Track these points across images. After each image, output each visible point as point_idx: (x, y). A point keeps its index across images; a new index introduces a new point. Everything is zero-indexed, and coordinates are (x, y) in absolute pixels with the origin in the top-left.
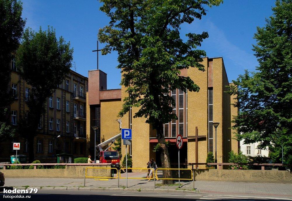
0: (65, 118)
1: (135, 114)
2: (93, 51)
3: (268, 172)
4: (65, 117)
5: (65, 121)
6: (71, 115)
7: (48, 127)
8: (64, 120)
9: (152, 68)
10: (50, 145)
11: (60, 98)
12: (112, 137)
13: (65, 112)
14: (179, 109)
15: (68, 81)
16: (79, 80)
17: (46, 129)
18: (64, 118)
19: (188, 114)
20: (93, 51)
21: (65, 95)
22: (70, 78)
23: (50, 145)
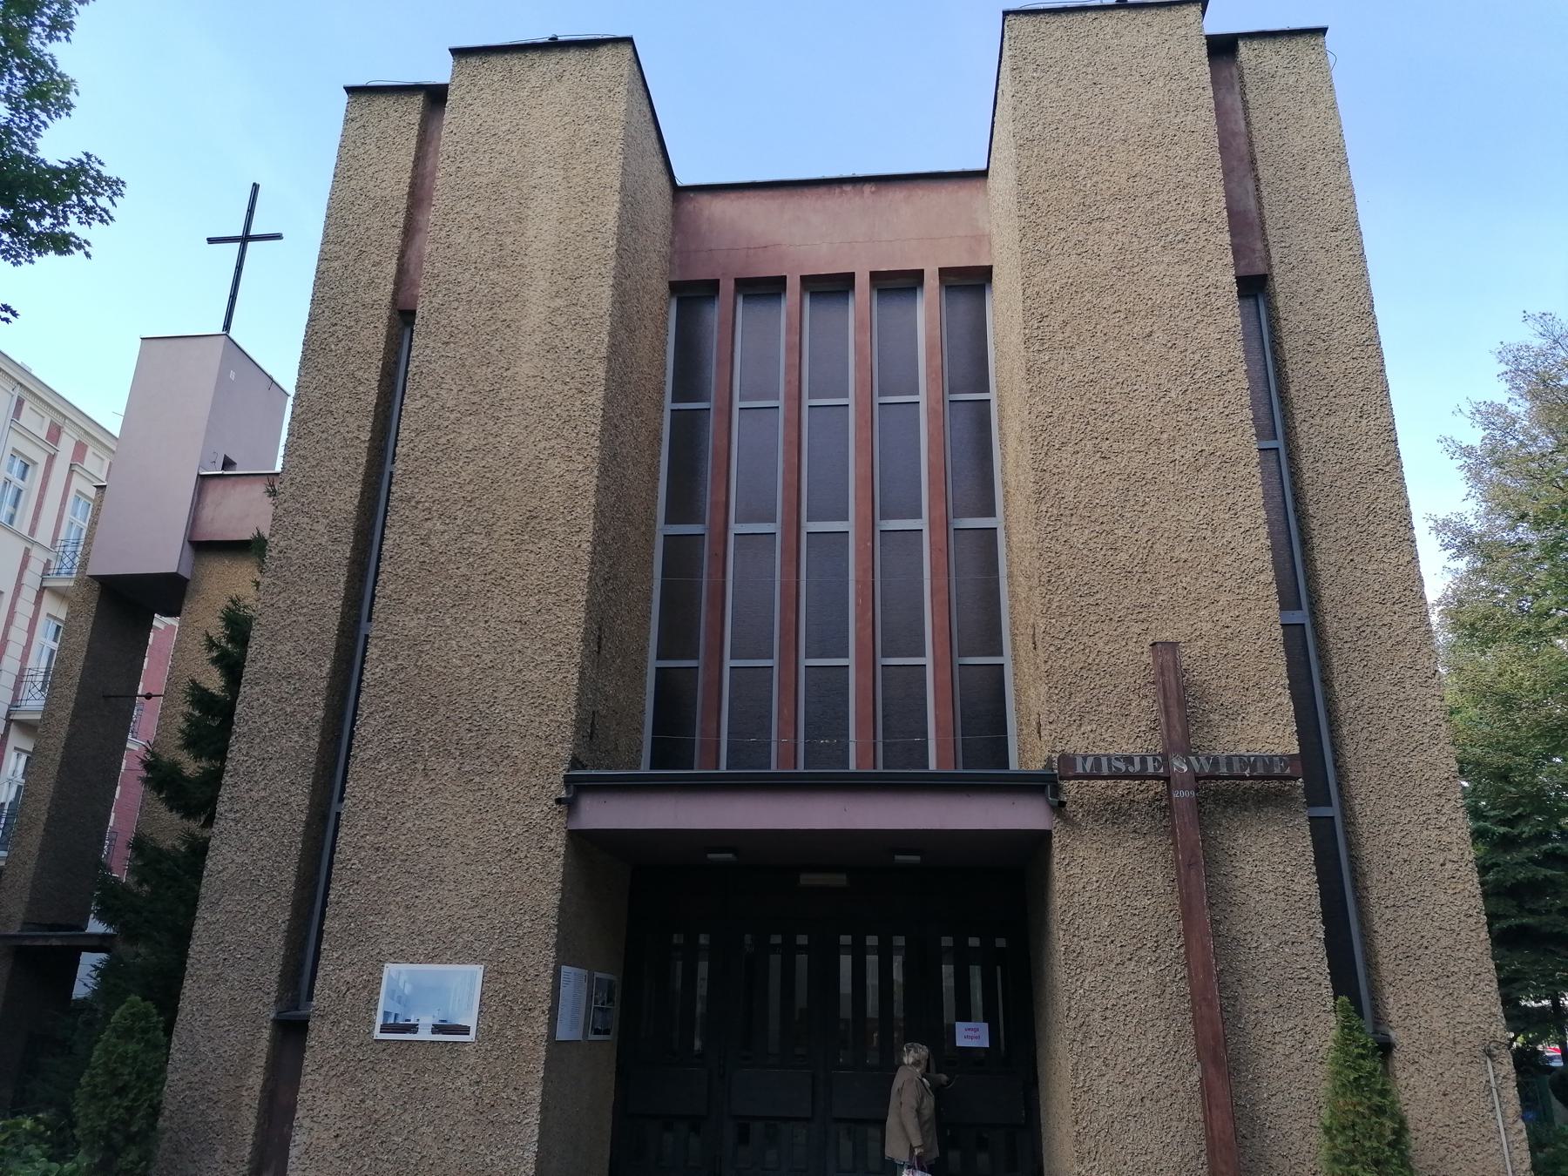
20: (278, 237)
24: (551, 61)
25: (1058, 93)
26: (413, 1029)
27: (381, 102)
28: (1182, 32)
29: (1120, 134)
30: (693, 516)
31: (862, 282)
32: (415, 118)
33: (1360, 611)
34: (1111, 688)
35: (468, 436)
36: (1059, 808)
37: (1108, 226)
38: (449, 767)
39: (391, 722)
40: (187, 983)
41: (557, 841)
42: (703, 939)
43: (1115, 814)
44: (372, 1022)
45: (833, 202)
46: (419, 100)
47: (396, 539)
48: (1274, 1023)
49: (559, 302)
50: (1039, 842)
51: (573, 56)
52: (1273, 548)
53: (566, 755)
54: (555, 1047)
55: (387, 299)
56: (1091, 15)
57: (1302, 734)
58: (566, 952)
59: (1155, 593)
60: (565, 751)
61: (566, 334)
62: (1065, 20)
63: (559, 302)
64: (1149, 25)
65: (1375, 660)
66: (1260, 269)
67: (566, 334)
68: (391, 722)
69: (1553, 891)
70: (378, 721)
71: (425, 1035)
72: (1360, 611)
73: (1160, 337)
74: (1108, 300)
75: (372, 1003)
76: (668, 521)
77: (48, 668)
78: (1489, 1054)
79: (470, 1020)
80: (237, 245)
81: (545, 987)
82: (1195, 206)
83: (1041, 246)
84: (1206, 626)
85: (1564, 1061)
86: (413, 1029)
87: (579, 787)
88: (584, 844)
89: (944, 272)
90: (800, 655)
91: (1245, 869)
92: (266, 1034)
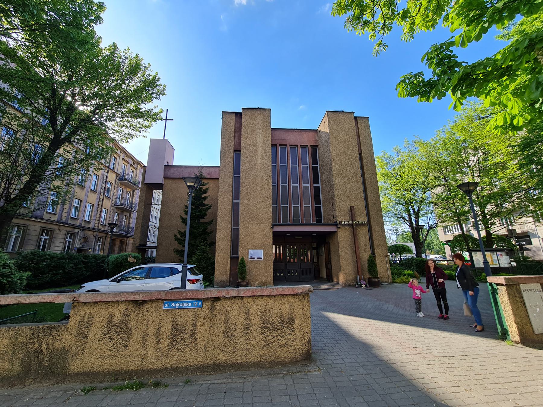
0: (102, 204)
1: (204, 218)
2: (173, 120)
3: (509, 307)
4: (102, 202)
5: (101, 208)
6: (112, 202)
7: (69, 212)
8: (100, 206)
9: (31, 271)
10: (68, 240)
11: (99, 176)
12: (322, 198)
13: (103, 196)
14: (233, 228)
15: (115, 158)
16: (131, 161)
17: (64, 214)
18: (100, 203)
19: (230, 239)
20: (173, 120)
21: (108, 173)
22: (119, 155)
23: (68, 240)
24: (258, 112)
26: (254, 258)
27: (228, 115)
32: (234, 118)
34: (388, 212)
35: (251, 173)
38: (254, 222)
39: (245, 216)
40: (216, 253)
41: (271, 233)
42: (295, 247)
44: (248, 258)
46: (234, 114)
47: (243, 189)
49: (263, 152)
51: (261, 111)
55: (233, 149)
60: (271, 220)
63: (263, 152)
68: (245, 216)
69: (464, 218)
70: (243, 216)
71: (256, 259)
75: (248, 255)
79: (262, 257)
80: (165, 121)
85: (416, 255)
86: (254, 258)
87: (273, 225)
88: (274, 233)
89: (311, 146)
90: (509, 274)
92: (229, 260)
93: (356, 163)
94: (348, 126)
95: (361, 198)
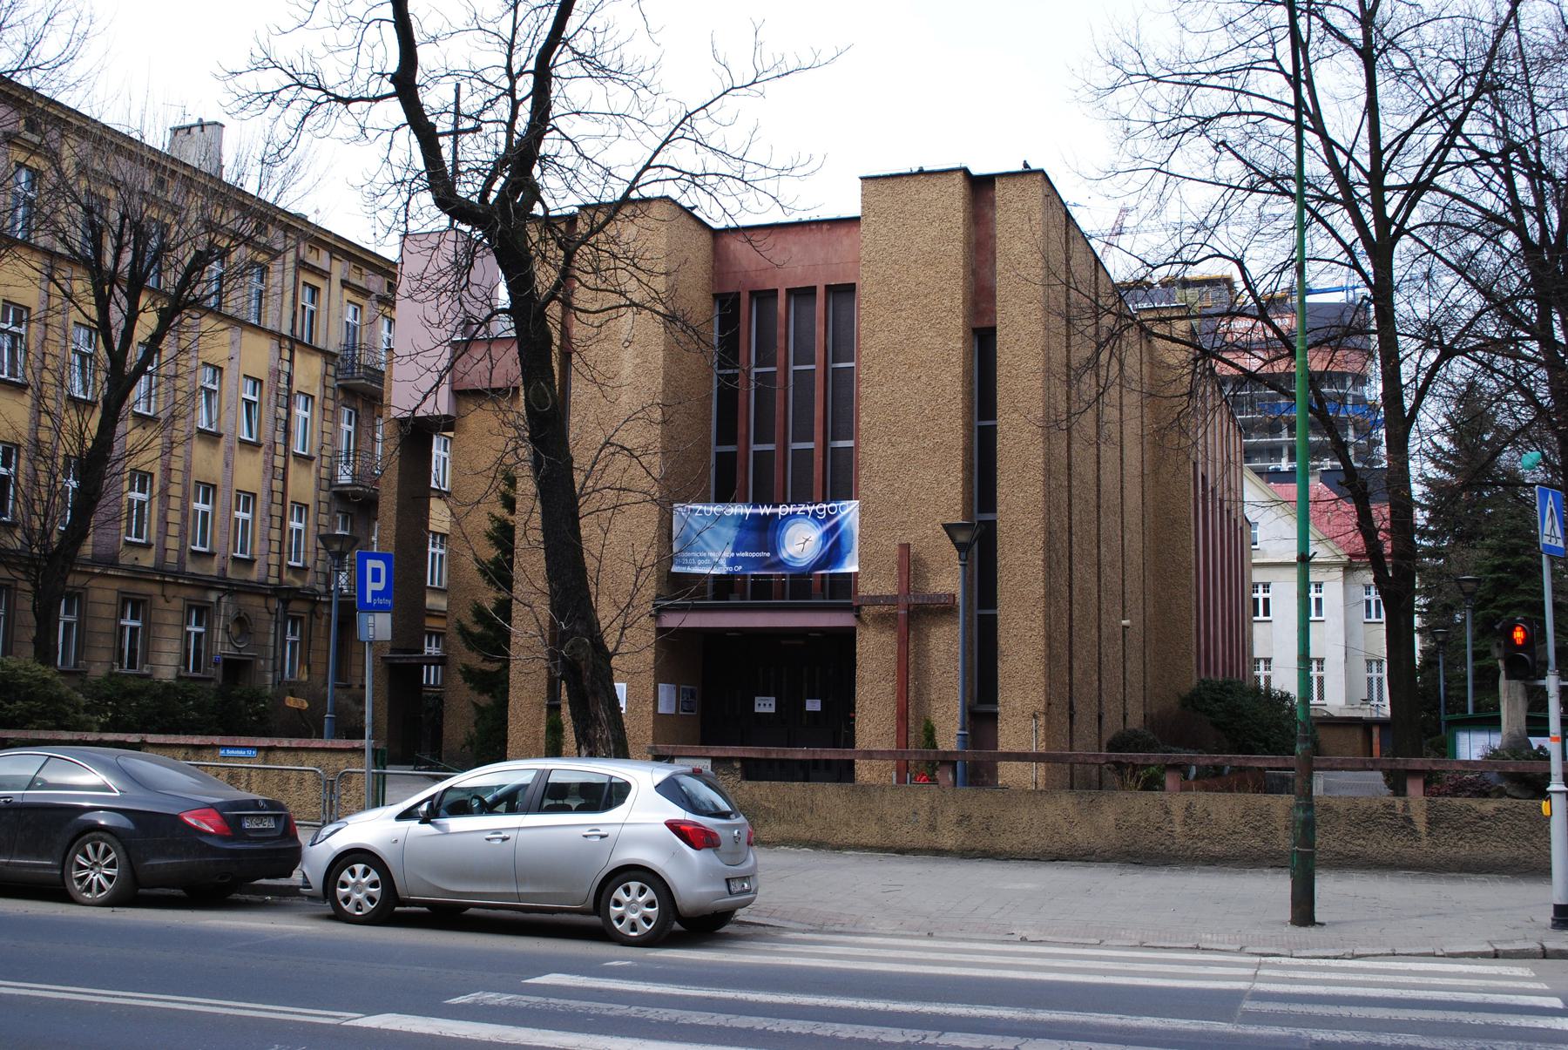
25: (884, 231)
28: (951, 190)
29: (913, 258)
30: (733, 441)
31: (821, 292)
33: (1013, 517)
36: (858, 617)
37: (903, 314)
43: (882, 620)
45: (806, 237)
48: (936, 705)
50: (854, 629)
52: (963, 493)
53: (654, 594)
54: (659, 718)
56: (905, 179)
57: (1307, 481)
58: (661, 676)
59: (909, 515)
61: (642, 379)
62: (891, 183)
64: (935, 185)
65: (1016, 541)
66: (986, 323)
67: (642, 379)
72: (1013, 517)
73: (924, 379)
74: (901, 358)
76: (718, 444)
77: (348, 449)
78: (1035, 716)
81: (651, 692)
82: (947, 303)
83: (871, 326)
84: (930, 532)
91: (933, 641)
93: (947, 378)
94: (933, 232)
95: (950, 507)
